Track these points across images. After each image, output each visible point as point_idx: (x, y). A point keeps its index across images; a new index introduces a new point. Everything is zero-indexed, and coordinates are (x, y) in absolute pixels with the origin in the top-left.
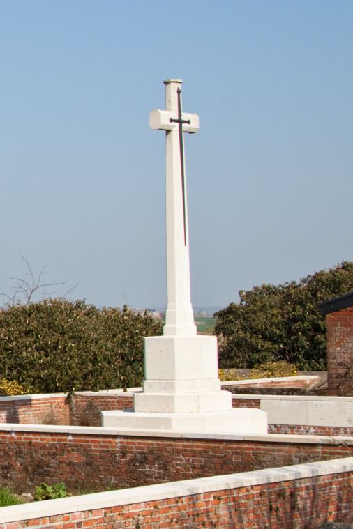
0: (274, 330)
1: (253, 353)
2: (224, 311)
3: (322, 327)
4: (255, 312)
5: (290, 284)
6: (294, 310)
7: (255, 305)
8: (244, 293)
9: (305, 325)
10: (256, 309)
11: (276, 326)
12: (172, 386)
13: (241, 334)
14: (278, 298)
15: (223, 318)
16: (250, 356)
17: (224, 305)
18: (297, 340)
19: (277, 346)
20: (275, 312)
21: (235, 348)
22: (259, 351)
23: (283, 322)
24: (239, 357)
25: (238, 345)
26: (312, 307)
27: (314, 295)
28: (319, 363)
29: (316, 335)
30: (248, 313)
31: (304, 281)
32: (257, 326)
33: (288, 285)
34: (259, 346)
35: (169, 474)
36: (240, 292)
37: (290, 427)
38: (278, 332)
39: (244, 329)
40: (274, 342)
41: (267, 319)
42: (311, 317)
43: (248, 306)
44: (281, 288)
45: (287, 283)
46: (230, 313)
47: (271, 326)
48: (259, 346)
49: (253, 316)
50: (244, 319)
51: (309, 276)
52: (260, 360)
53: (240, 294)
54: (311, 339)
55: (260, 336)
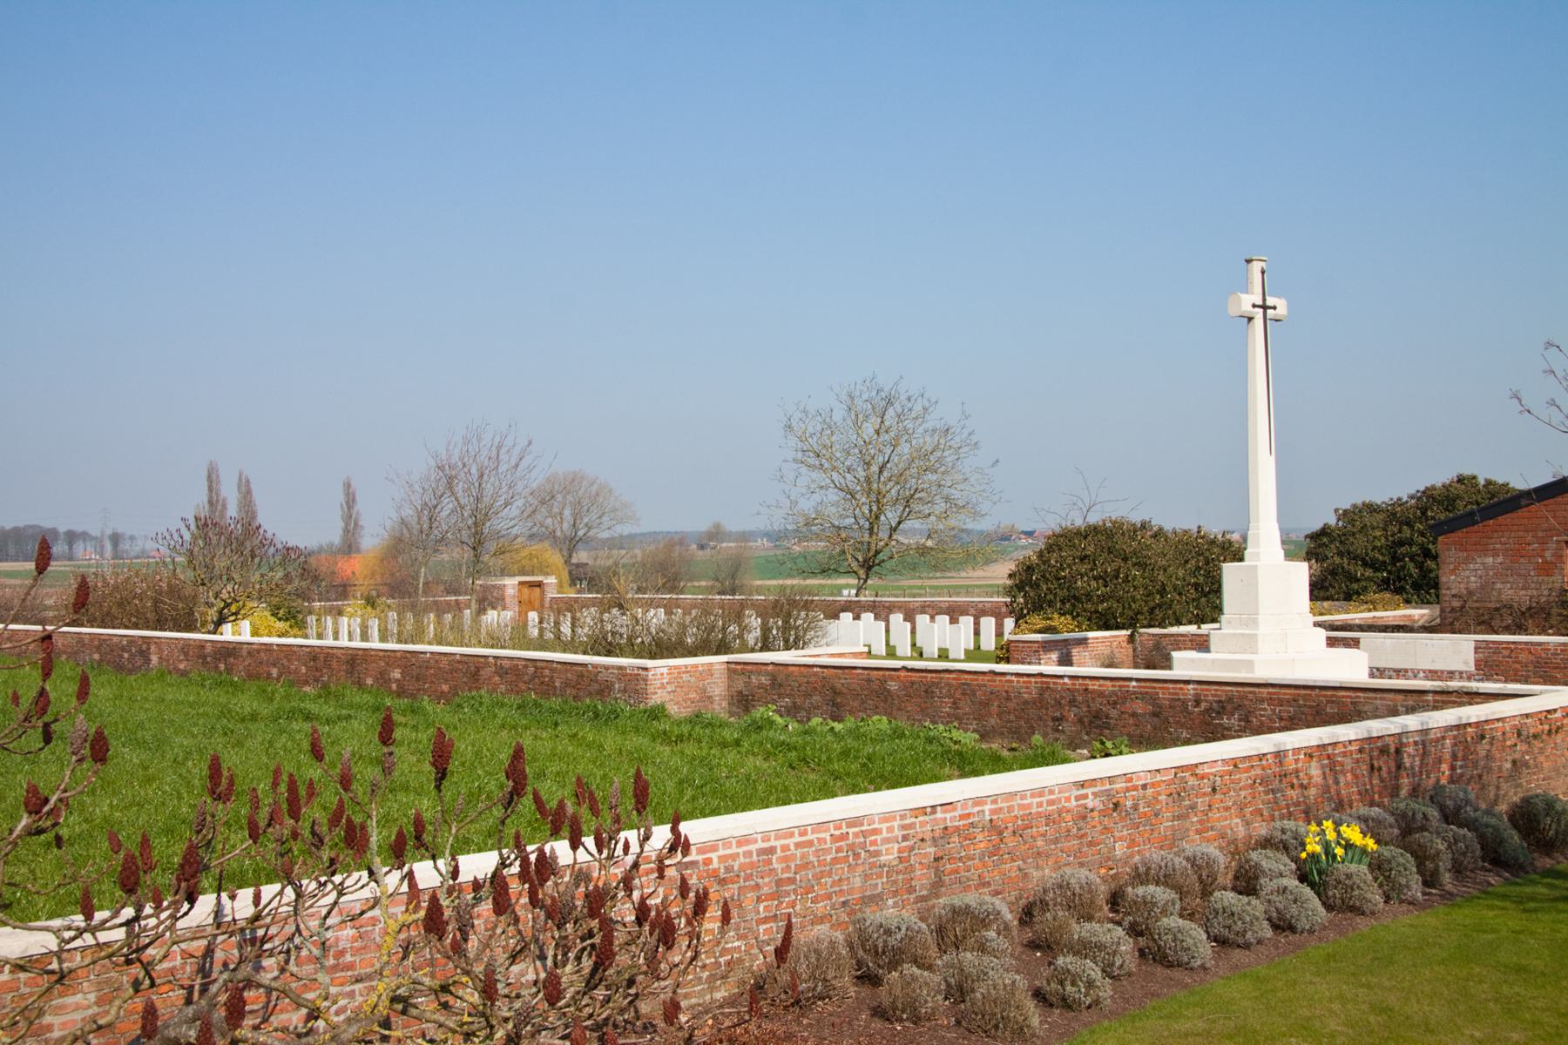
1: (1351, 583)
4: (1354, 534)
7: (1354, 526)
8: (1341, 512)
10: (1355, 530)
13: (1337, 560)
14: (1380, 517)
16: (1347, 587)
17: (1316, 526)
18: (1403, 568)
22: (1358, 580)
28: (1430, 594)
31: (1412, 497)
36: (1336, 511)
38: (1381, 558)
39: (1341, 554)
40: (1376, 570)
47: (1372, 550)
49: (1351, 539)
54: (1420, 566)
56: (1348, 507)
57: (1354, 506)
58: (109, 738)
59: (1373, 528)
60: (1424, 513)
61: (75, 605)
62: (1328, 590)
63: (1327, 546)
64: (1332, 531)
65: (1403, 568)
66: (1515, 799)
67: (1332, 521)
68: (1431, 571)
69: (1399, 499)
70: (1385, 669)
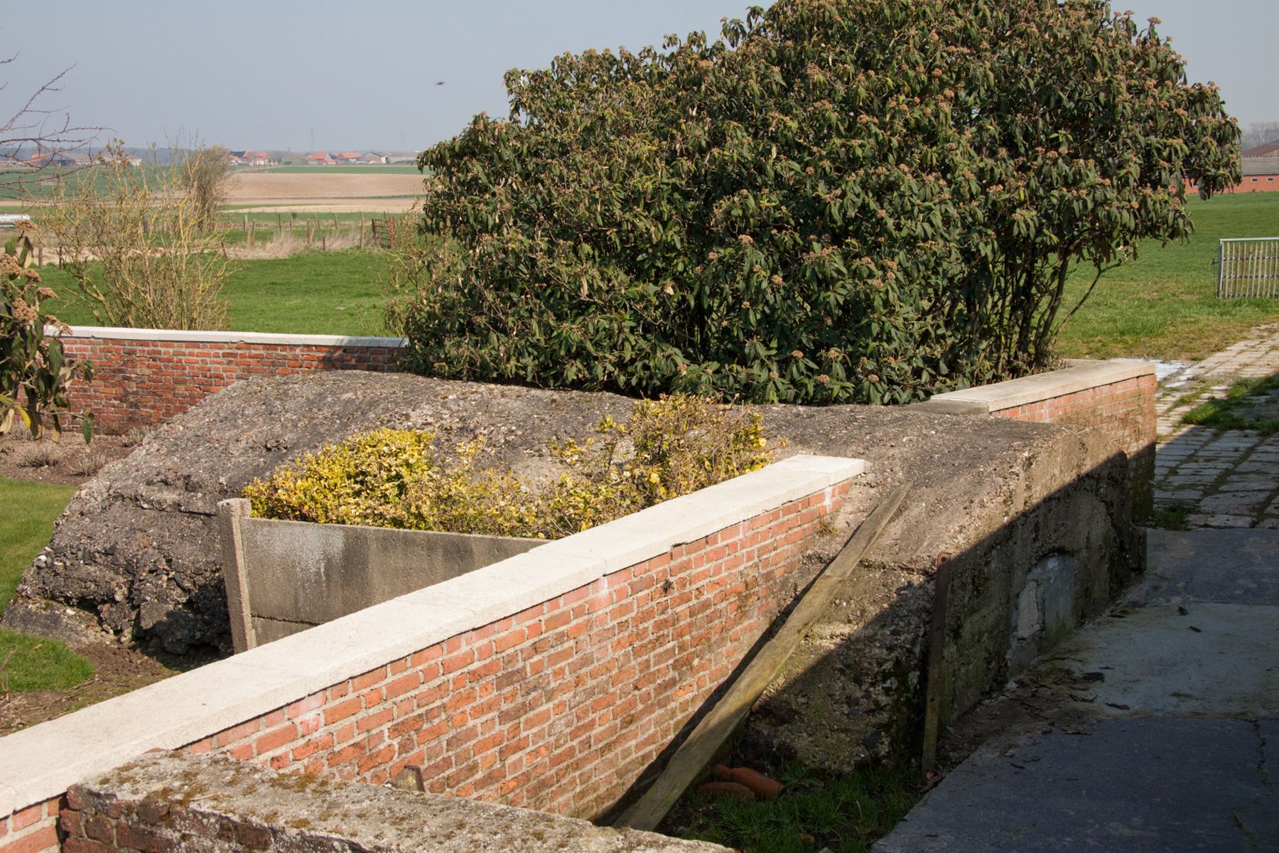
0: (641, 225)
1: (560, 318)
2: (452, 149)
3: (835, 210)
4: (564, 150)
5: (684, 41)
6: (718, 138)
7: (563, 123)
8: (524, 81)
9: (764, 203)
10: (564, 136)
11: (648, 207)
12: (259, 644)
13: (515, 238)
14: (644, 95)
15: (451, 174)
16: (547, 330)
17: (452, 130)
18: (730, 267)
19: (652, 288)
20: (644, 149)
21: (490, 296)
22: (582, 308)
23: (675, 188)
24: (505, 331)
25: (502, 282)
26: (794, 125)
27: (793, 69)
28: (825, 367)
29: (808, 248)
30: (536, 154)
31: (733, 31)
32: (574, 205)
33: (675, 49)
34: (585, 290)
35: (275, 734)
36: (510, 78)
37: (316, 346)
38: (656, 233)
39: (525, 218)
40: (638, 272)
41: (610, 178)
42: (790, 169)
43: (539, 129)
44: (649, 61)
45: (672, 41)
46: (473, 155)
47: (627, 204)
48: (585, 290)
49: (558, 167)
50: (526, 176)
51: (754, 12)
52: (589, 346)
53: (508, 80)
54: (787, 262)
55: (587, 248)
56: (545, 66)
57: (564, 64)
58: (429, 380)
59: (624, 130)
60: (793, 69)
61: (1255, 388)
62: (486, 341)
63: (484, 190)
64: (498, 140)
65: (730, 267)
66: (760, 663)
67: (499, 109)
68: (826, 282)
69: (695, 39)
70: (540, 382)
